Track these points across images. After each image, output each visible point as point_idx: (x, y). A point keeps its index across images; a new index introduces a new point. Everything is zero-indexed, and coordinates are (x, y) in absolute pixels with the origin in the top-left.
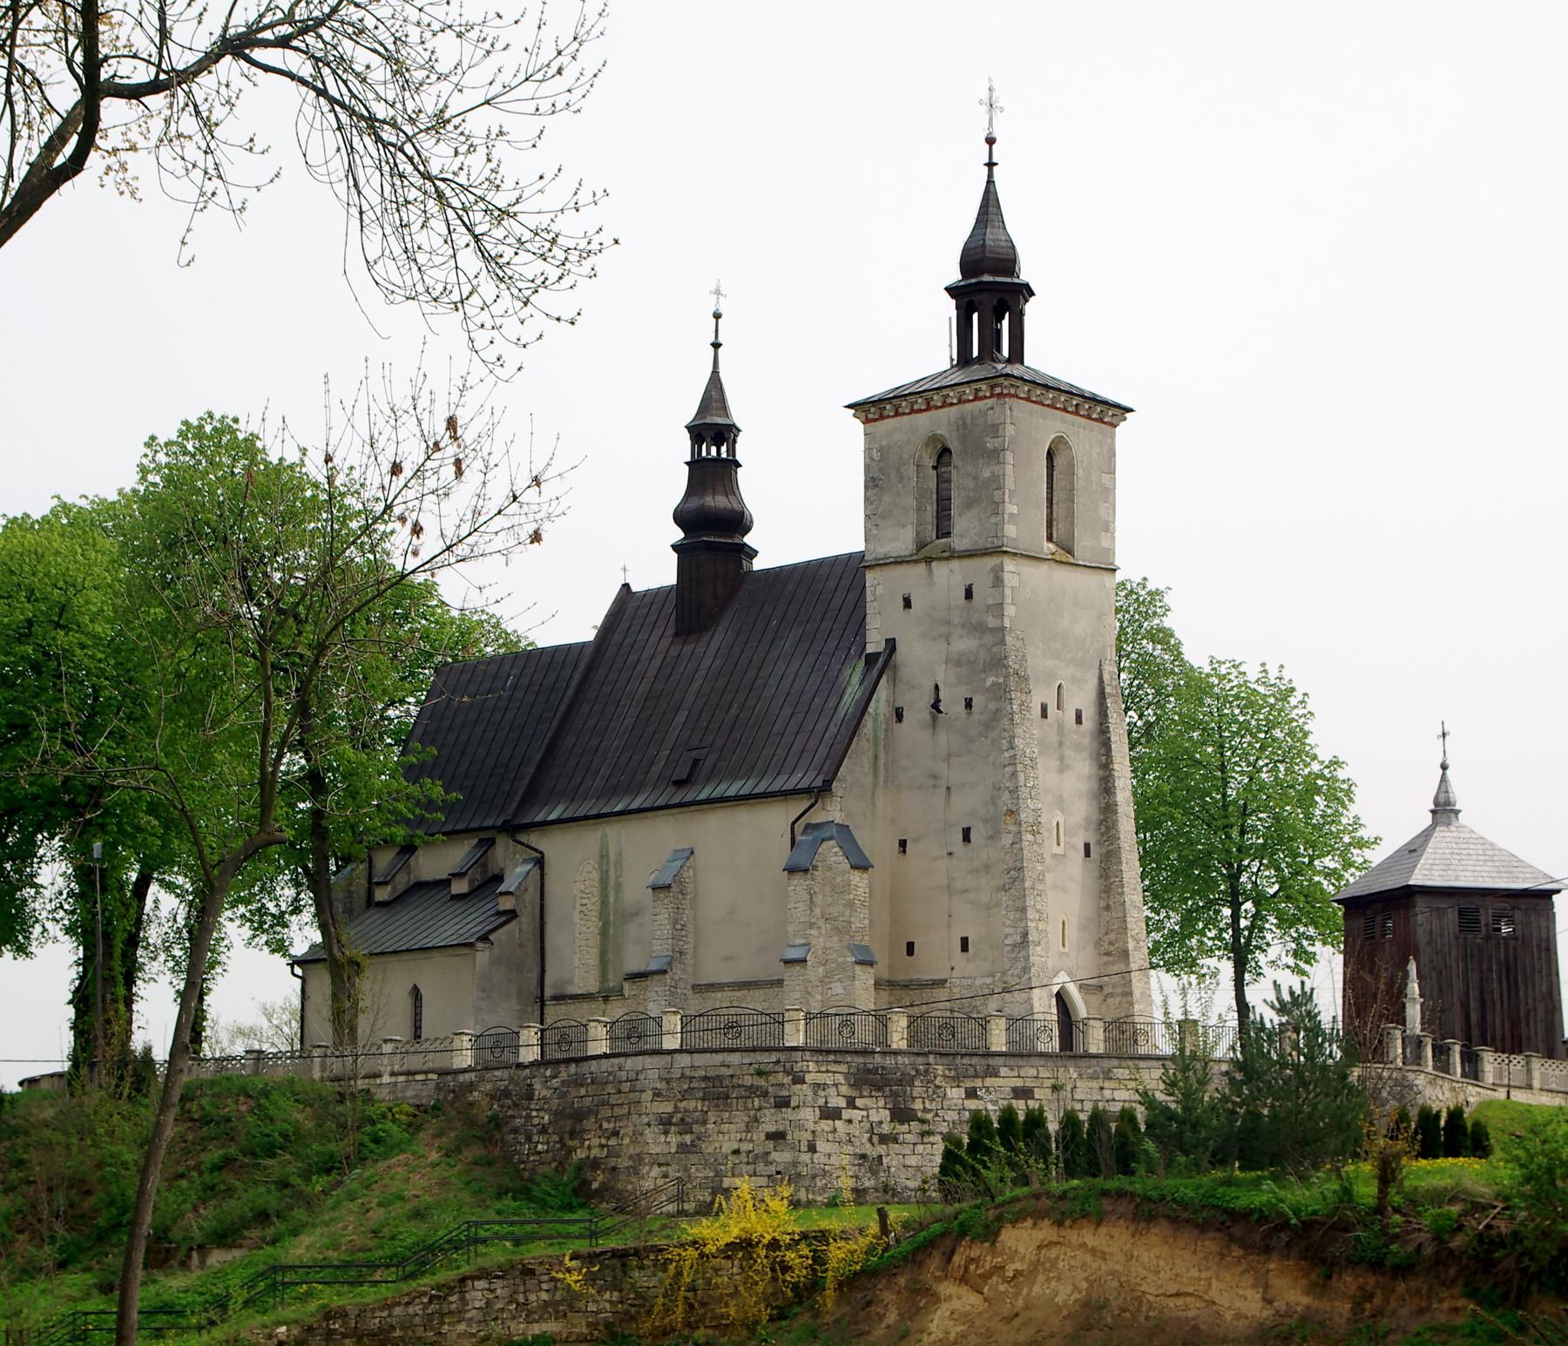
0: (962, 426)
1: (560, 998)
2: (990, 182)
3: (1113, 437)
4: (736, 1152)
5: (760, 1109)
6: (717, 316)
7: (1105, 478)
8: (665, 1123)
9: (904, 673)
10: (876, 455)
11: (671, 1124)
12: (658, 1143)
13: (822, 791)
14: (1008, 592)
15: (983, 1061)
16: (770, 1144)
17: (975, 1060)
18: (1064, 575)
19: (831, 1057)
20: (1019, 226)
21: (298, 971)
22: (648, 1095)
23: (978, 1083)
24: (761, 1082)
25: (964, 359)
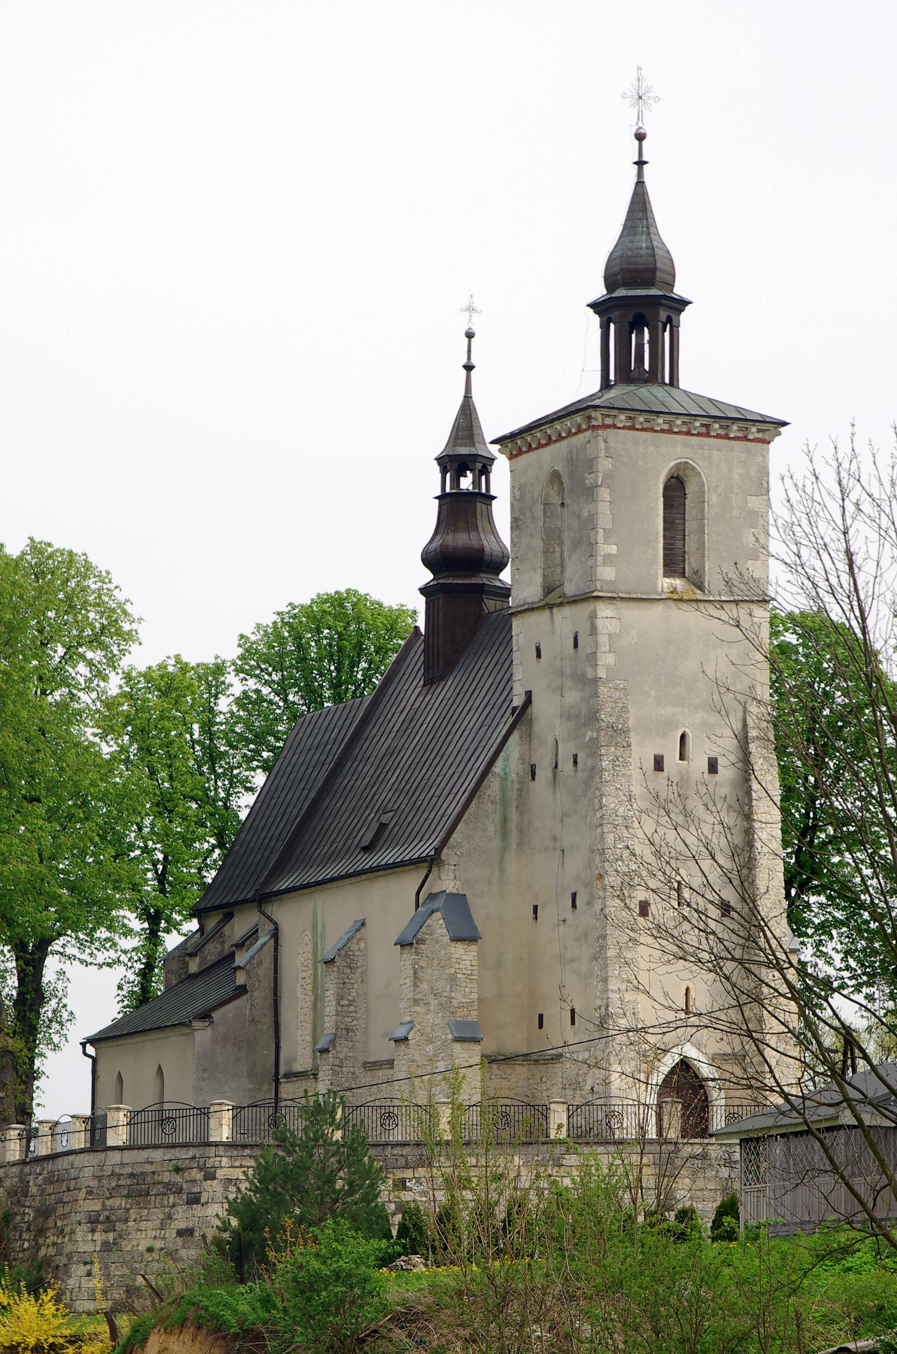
0: (571, 461)
1: (289, 1075)
2: (640, 184)
3: (765, 455)
4: (150, 1250)
5: (174, 1206)
6: (470, 335)
7: (754, 502)
8: (93, 1221)
9: (536, 727)
10: (517, 493)
11: (98, 1222)
12: (86, 1242)
13: (433, 861)
14: (603, 640)
15: (417, 1151)
16: (179, 1241)
17: (406, 1151)
18: (689, 618)
19: (247, 1152)
20: (672, 230)
21: (90, 1050)
22: (82, 1194)
23: (409, 1174)
24: (178, 1179)
25: (606, 384)
